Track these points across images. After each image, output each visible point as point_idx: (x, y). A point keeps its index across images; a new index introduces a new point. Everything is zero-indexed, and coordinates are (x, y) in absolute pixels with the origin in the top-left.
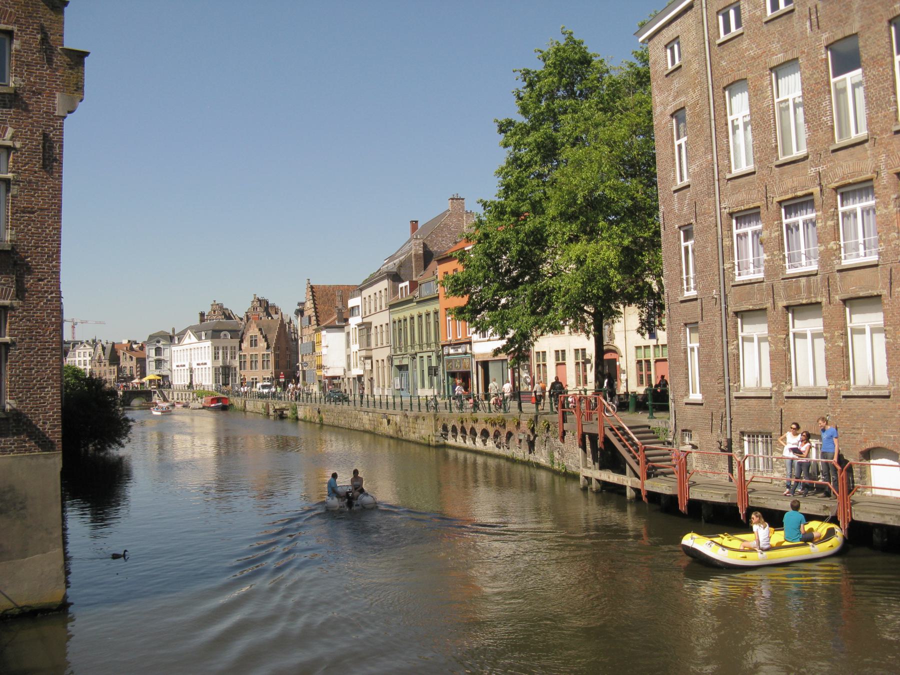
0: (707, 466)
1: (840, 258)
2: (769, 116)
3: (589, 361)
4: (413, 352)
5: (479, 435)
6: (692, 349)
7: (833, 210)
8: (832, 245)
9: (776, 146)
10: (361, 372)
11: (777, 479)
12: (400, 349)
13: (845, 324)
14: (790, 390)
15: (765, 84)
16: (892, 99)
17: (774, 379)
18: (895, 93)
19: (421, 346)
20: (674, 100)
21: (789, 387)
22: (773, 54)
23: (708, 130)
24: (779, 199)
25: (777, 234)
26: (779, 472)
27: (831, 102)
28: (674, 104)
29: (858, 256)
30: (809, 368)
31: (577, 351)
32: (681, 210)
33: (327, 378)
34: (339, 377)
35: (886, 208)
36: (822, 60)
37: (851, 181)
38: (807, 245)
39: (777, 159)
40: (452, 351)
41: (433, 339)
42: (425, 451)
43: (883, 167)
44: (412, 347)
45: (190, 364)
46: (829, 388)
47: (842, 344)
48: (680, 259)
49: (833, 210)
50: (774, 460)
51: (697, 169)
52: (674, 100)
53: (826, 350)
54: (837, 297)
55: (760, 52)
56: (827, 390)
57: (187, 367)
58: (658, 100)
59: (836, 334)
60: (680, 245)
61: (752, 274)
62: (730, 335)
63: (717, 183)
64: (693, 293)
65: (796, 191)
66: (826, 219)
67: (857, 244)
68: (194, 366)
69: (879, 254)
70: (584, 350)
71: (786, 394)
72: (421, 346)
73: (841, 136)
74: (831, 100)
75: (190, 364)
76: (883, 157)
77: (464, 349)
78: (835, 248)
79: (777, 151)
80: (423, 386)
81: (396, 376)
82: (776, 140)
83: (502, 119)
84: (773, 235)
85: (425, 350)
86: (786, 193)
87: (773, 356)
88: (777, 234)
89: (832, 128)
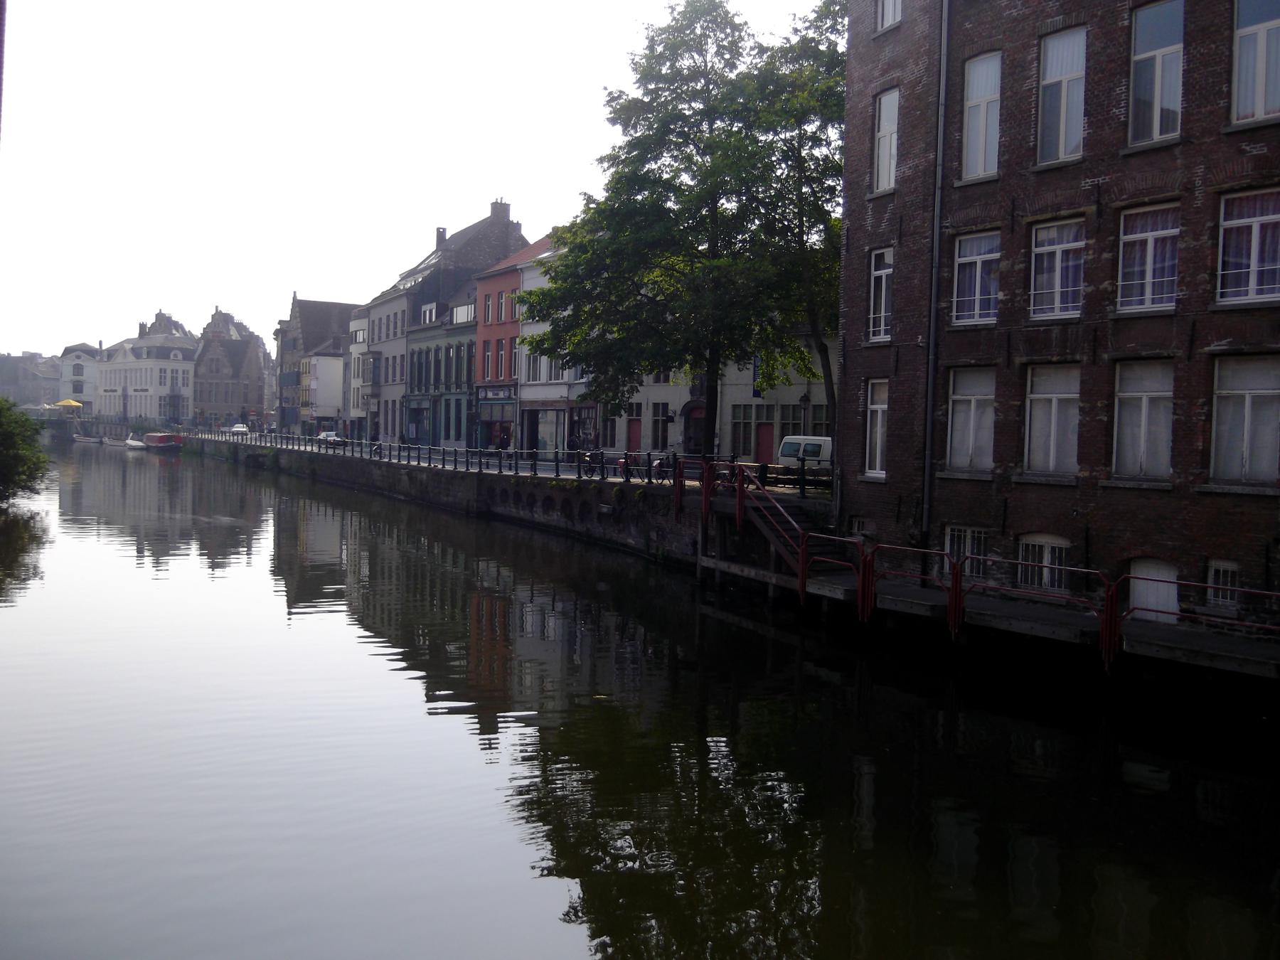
0: (886, 565)
1: (1115, 304)
2: (1030, 103)
3: (671, 419)
4: (437, 393)
5: (539, 504)
6: (874, 412)
7: (1112, 238)
8: (1106, 284)
9: (1035, 145)
10: (363, 414)
11: (992, 589)
12: (419, 390)
13: (1113, 392)
14: (1021, 474)
15: (1029, 58)
16: (1225, 89)
17: (998, 457)
18: (1229, 82)
19: (448, 388)
20: (882, 75)
21: (1019, 470)
22: (1049, 16)
23: (934, 119)
24: (1030, 219)
25: (1022, 266)
26: (996, 579)
27: (1128, 89)
28: (882, 80)
29: (1142, 302)
30: (1052, 441)
31: (656, 405)
32: (876, 225)
33: (313, 418)
34: (332, 419)
35: (1197, 239)
36: (1123, 28)
37: (1146, 199)
38: (985, 291)
39: (1035, 164)
40: (490, 395)
41: (464, 378)
42: (130, 489)
43: (1198, 182)
44: (436, 388)
45: (125, 389)
46: (1080, 475)
47: (1105, 419)
48: (869, 292)
49: (1112, 238)
50: (990, 563)
51: (909, 173)
52: (882, 75)
53: (1081, 425)
54: (1106, 356)
55: (1027, 11)
56: (1077, 478)
57: (120, 392)
58: (856, 75)
59: (1099, 404)
60: (869, 274)
61: (976, 319)
62: (940, 395)
63: (938, 193)
64: (884, 338)
65: (1059, 209)
66: (1103, 250)
67: (1142, 286)
68: (130, 392)
69: (1178, 301)
70: (665, 405)
71: (1014, 479)
72: (448, 388)
73: (1136, 138)
74: (1128, 86)
75: (125, 389)
76: (1200, 170)
77: (507, 394)
78: (1110, 289)
79: (1035, 154)
80: (447, 437)
81: (410, 422)
82: (1036, 138)
83: (614, 88)
84: (1017, 267)
85: (453, 391)
86: (1042, 211)
87: (999, 428)
88: (1022, 266)
89: (1125, 124)
